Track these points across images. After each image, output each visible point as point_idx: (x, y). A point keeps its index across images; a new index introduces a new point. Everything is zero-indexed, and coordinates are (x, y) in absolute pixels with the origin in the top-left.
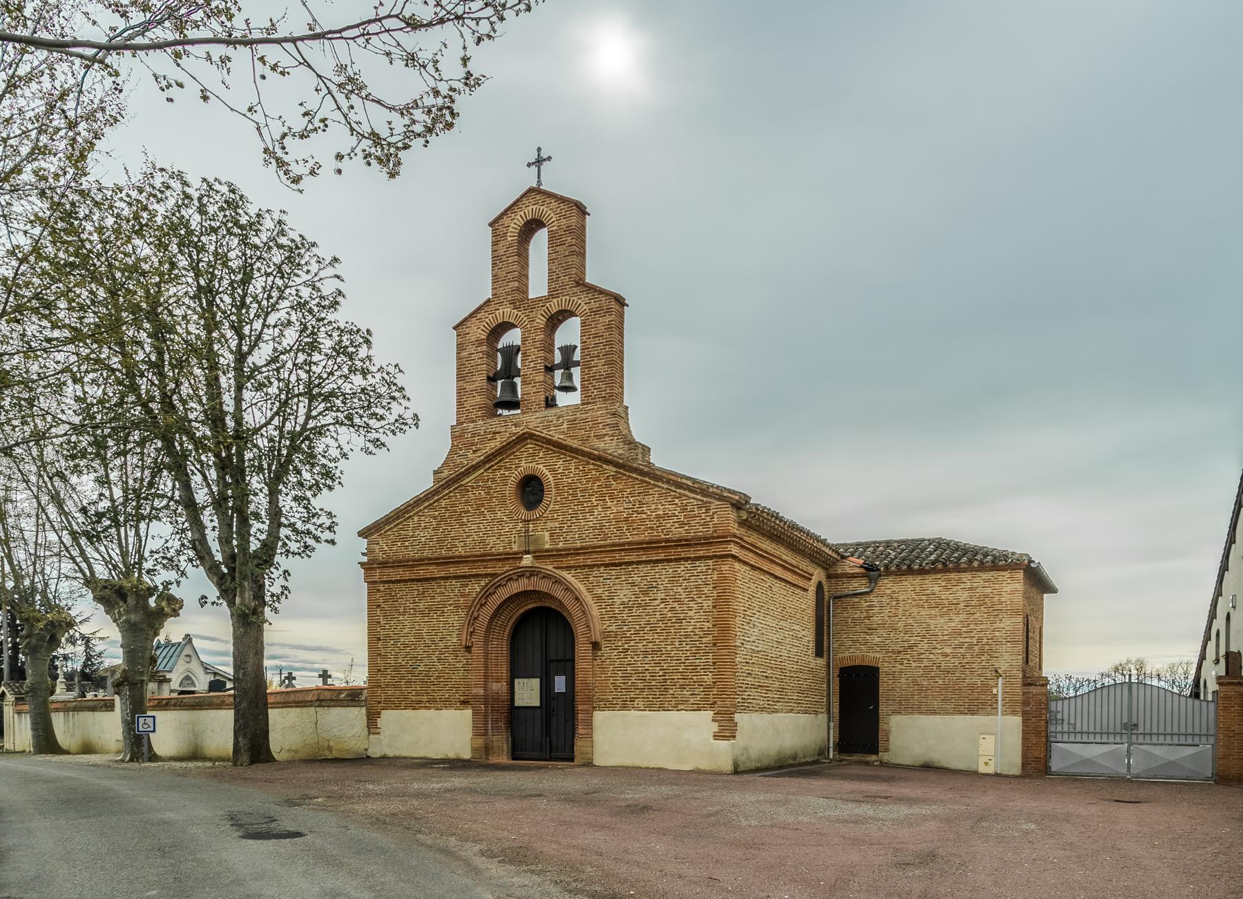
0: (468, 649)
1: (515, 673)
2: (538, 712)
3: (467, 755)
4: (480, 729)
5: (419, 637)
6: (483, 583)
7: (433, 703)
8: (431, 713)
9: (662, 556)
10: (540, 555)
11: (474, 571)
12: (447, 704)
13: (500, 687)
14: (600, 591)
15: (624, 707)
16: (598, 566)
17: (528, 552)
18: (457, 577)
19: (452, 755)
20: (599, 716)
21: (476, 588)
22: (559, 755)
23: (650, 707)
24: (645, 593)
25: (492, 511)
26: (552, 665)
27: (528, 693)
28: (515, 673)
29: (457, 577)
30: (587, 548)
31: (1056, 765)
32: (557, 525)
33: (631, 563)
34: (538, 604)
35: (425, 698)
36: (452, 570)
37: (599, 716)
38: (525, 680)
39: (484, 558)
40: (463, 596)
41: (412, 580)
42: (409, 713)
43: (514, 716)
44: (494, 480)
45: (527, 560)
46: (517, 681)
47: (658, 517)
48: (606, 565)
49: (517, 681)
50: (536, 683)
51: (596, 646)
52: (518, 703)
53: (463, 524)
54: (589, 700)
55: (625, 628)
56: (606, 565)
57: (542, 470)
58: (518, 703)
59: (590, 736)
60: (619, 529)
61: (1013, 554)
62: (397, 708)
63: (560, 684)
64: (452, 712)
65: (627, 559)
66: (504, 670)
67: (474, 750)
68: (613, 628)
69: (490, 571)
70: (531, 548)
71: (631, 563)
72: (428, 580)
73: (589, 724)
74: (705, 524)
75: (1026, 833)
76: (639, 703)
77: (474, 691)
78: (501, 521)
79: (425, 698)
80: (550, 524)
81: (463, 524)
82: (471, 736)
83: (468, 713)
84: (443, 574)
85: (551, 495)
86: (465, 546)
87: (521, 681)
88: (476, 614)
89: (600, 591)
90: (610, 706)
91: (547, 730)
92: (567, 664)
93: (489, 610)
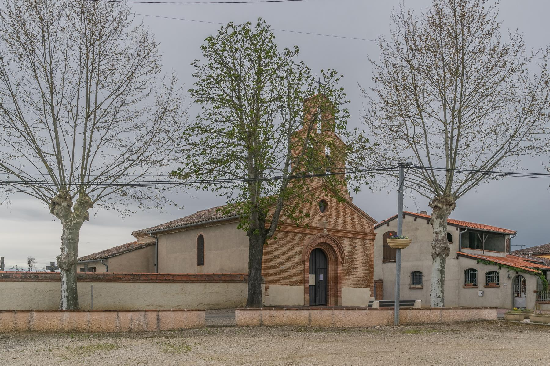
2: (314, 287)
3: (302, 304)
5: (284, 256)
7: (289, 283)
8: (288, 287)
9: (359, 237)
11: (306, 232)
12: (294, 283)
15: (349, 286)
19: (297, 304)
20: (343, 289)
23: (355, 286)
24: (354, 248)
31: (266, 301)
33: (350, 238)
35: (286, 281)
37: (343, 289)
40: (300, 241)
41: (284, 232)
42: (280, 287)
47: (357, 224)
48: (345, 237)
54: (341, 284)
56: (345, 237)
57: (327, 199)
61: (62, 223)
62: (275, 284)
64: (296, 287)
65: (351, 236)
71: (350, 238)
72: (288, 232)
74: (368, 229)
75: (527, 317)
76: (352, 285)
79: (286, 281)
84: (295, 231)
85: (330, 209)
90: (345, 286)
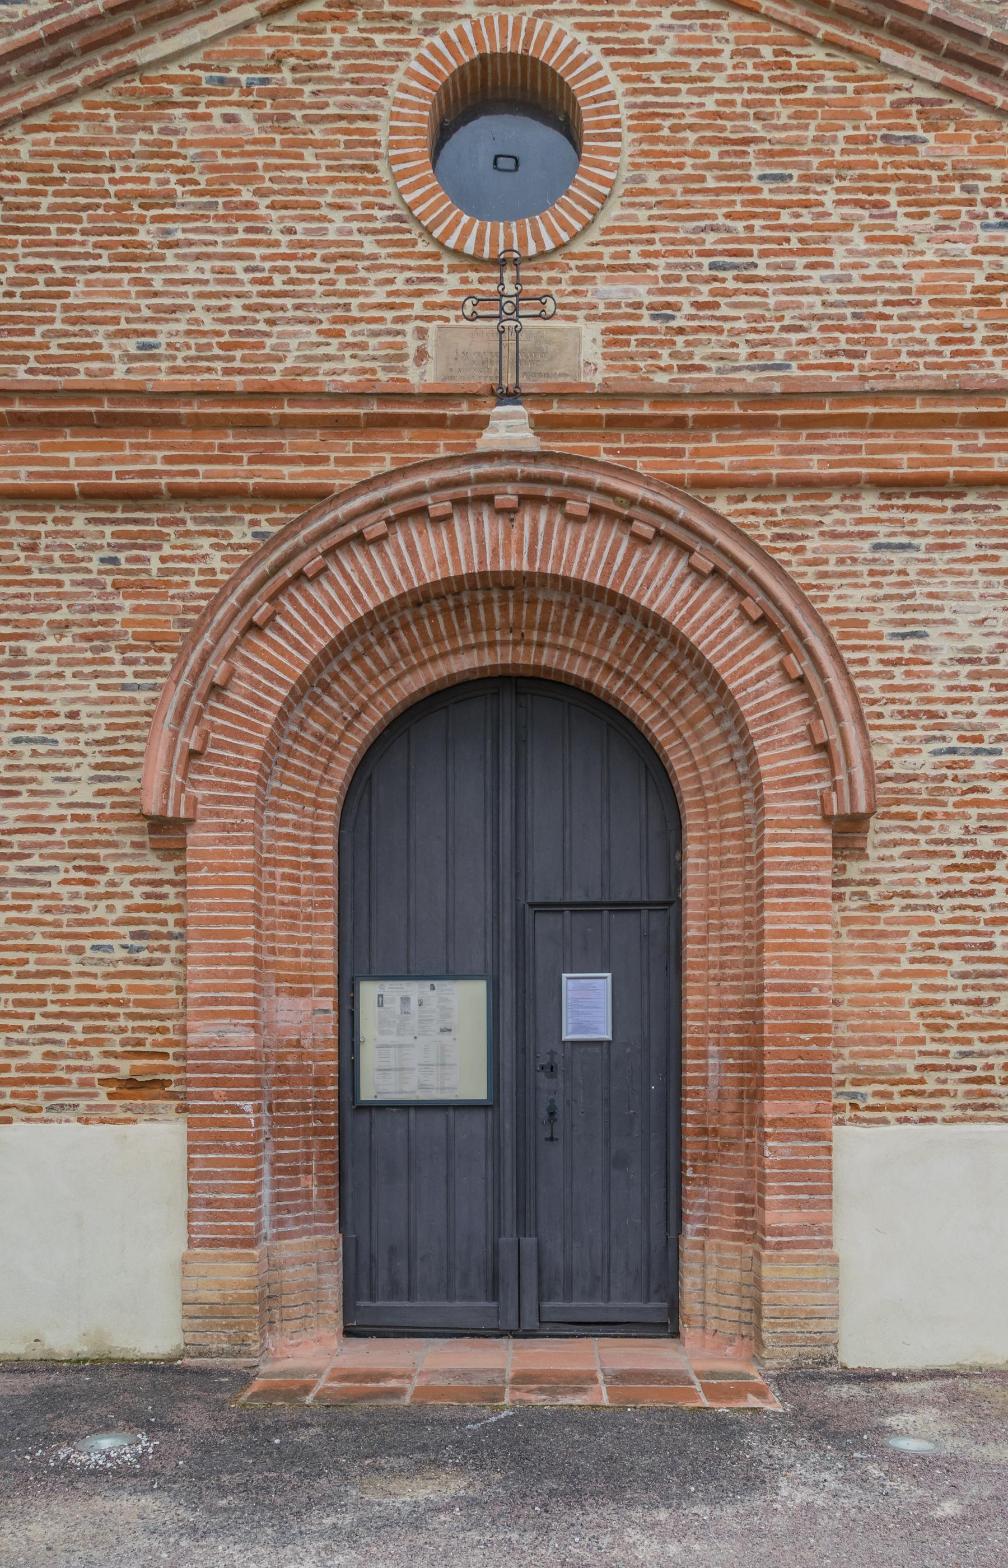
0: (166, 831)
1: (361, 957)
4: (215, 1223)
6: (241, 533)
10: (563, 411)
13: (303, 1017)
14: (857, 598)
16: (850, 485)
17: (511, 396)
18: (98, 496)
20: (860, 1150)
21: (207, 554)
22: (581, 1306)
25: (294, 202)
26: (546, 924)
27: (429, 1040)
28: (361, 957)
29: (98, 496)
30: (816, 397)
32: (642, 292)
34: (503, 657)
36: (77, 459)
37: (860, 1150)
38: (414, 989)
39: (258, 411)
43: (360, 1146)
44: (309, 65)
45: (509, 429)
46: (368, 991)
48: (889, 486)
49: (368, 991)
50: (466, 1001)
51: (848, 831)
52: (372, 1087)
53: (131, 255)
54: (814, 1077)
55: (981, 765)
56: (889, 486)
58: (372, 1087)
59: (819, 1236)
60: (953, 336)
63: (587, 1005)
64: (62, 1135)
66: (323, 937)
67: (199, 1312)
68: (924, 761)
69: (288, 475)
70: (528, 384)
73: (816, 1185)
77: (201, 1033)
78: (345, 256)
80: (606, 290)
81: (131, 255)
82: (174, 1243)
83: (160, 1139)
86: (148, 352)
87: (394, 990)
88: (218, 670)
89: (857, 598)
90: (909, 1101)
91: (520, 1197)
92: (644, 926)
93: (282, 658)
